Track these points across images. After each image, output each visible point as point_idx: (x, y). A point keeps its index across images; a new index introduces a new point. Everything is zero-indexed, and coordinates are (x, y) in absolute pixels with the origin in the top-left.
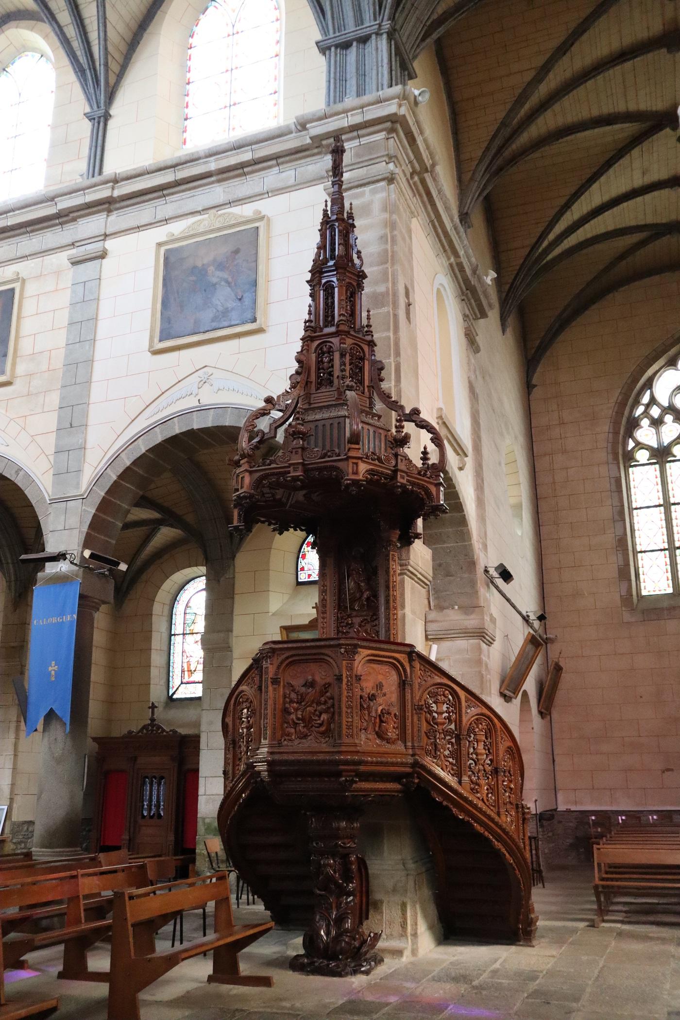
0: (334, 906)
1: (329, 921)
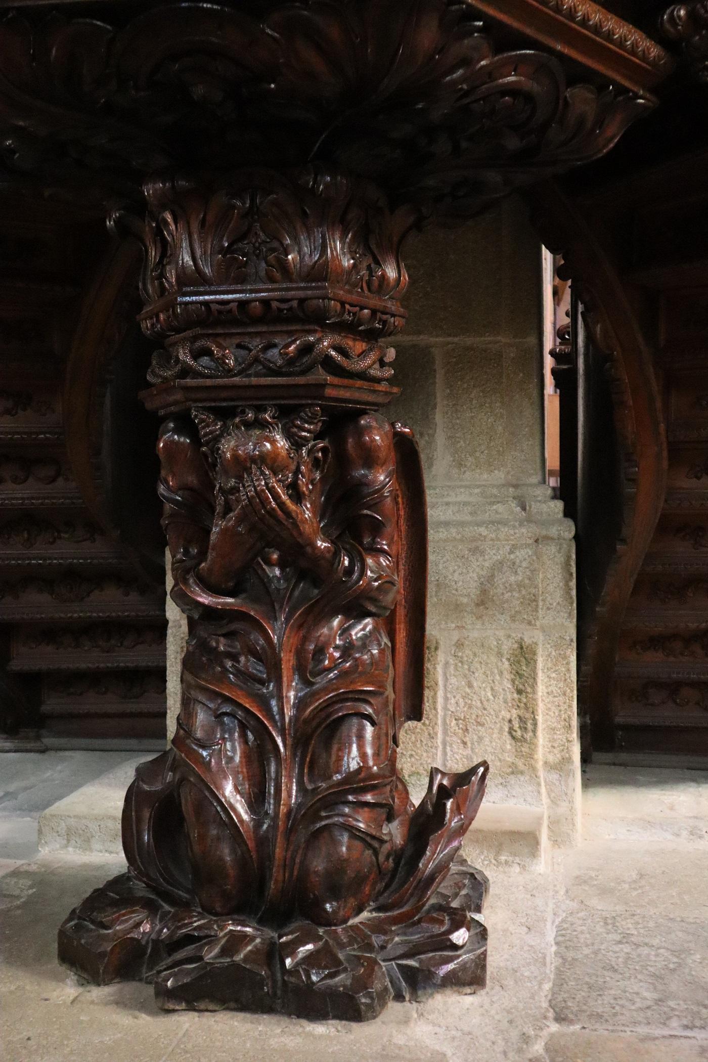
0: (288, 661)
1: (263, 735)
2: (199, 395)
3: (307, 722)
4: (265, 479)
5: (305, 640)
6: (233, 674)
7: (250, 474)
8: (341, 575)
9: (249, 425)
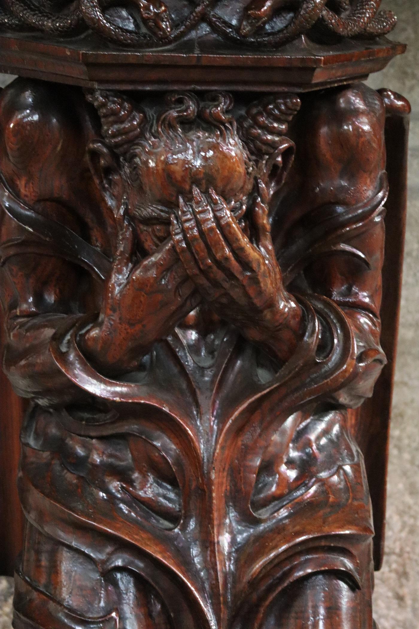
2: (113, 75)
3: (254, 583)
4: (213, 211)
5: (247, 451)
6: (125, 503)
7: (189, 198)
8: (314, 354)
9: (187, 124)
